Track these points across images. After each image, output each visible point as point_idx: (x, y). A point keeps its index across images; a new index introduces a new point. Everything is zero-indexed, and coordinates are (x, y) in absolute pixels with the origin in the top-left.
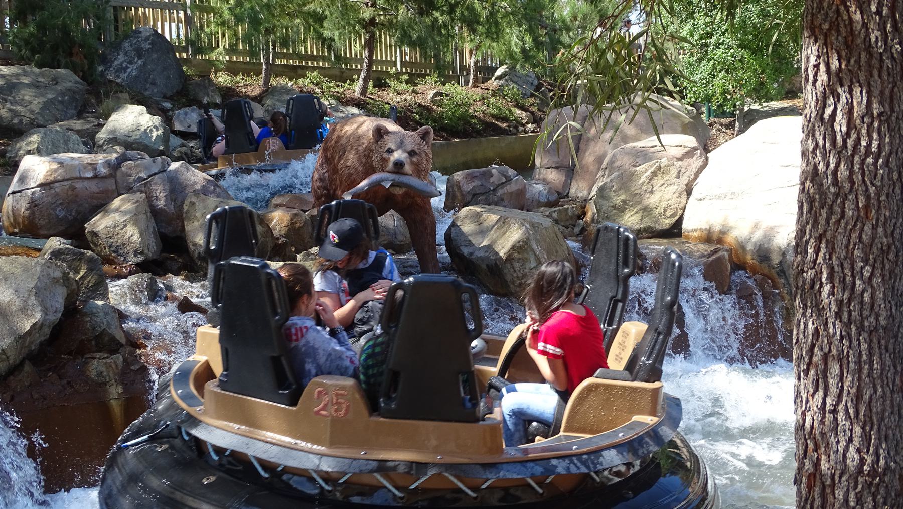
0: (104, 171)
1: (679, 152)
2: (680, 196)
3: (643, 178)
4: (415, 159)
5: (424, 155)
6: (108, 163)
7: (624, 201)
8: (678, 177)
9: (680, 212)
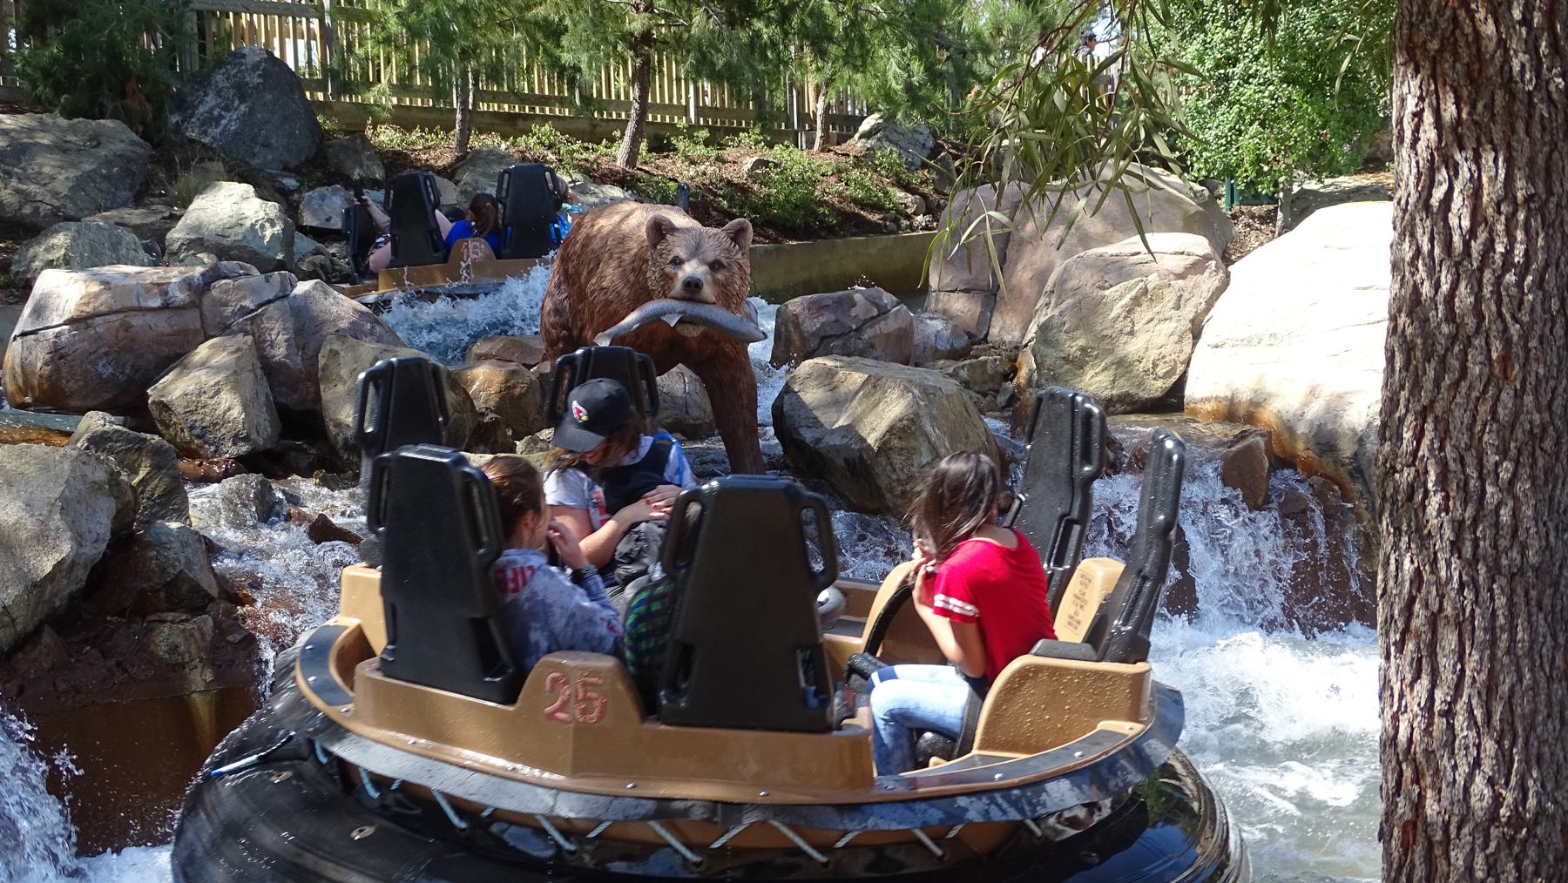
0: (180, 296)
1: (1179, 264)
2: (1180, 341)
3: (1117, 309)
4: (720, 276)
5: (736, 269)
6: (187, 283)
7: (1083, 349)
8: (1177, 307)
9: (1180, 368)
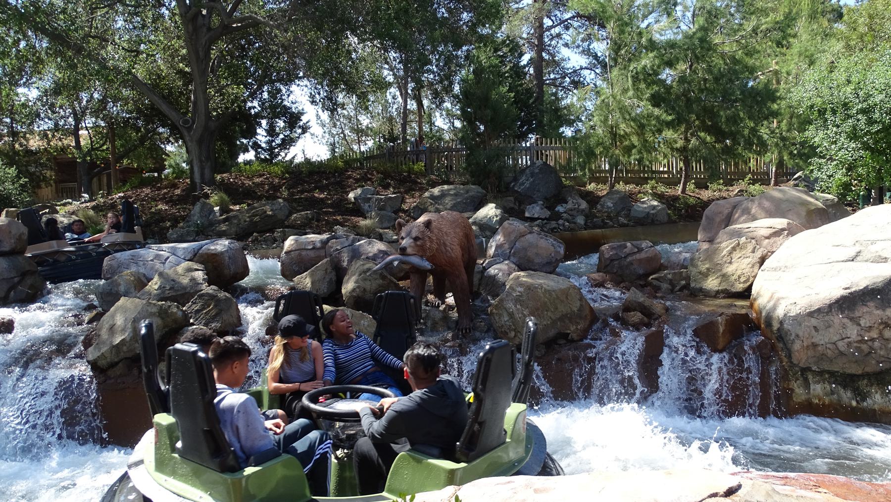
0: (319, 245)
1: (768, 232)
2: (753, 266)
3: (725, 252)
4: (418, 243)
5: (427, 239)
6: (322, 241)
7: (708, 269)
8: (753, 252)
9: (751, 279)
